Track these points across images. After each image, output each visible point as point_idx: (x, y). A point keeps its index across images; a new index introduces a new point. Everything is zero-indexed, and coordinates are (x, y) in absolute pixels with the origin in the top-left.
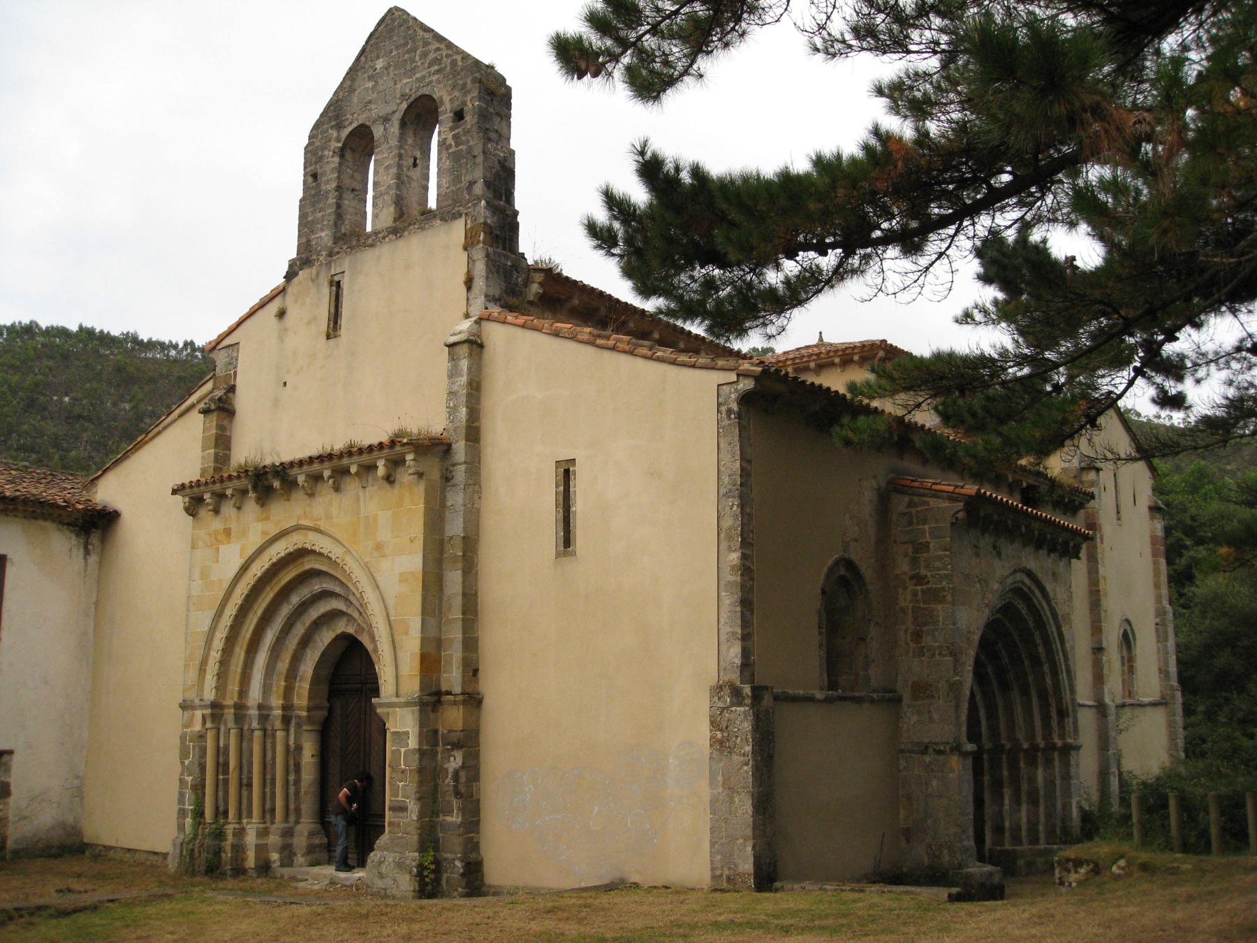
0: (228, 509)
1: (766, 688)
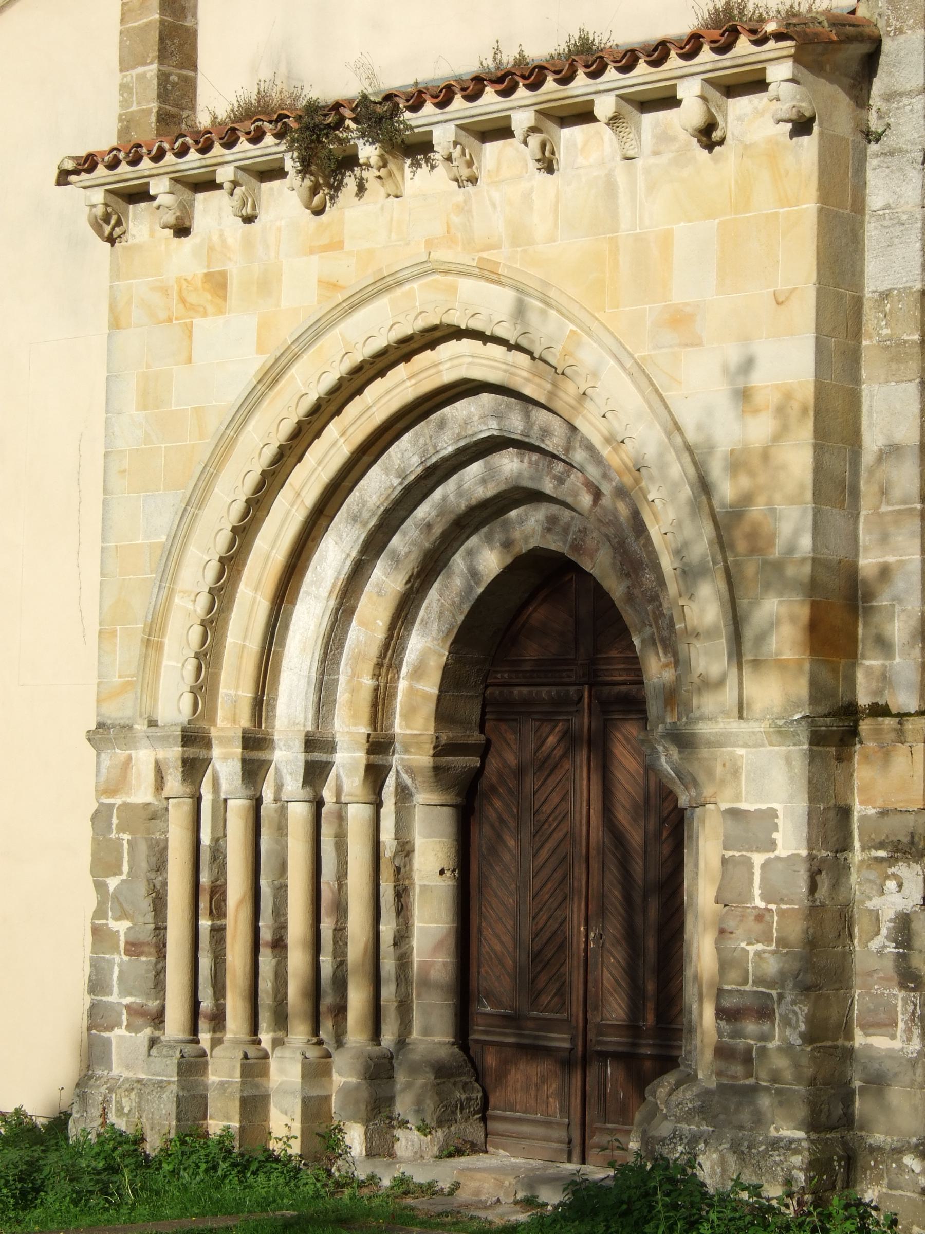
0: (213, 212)
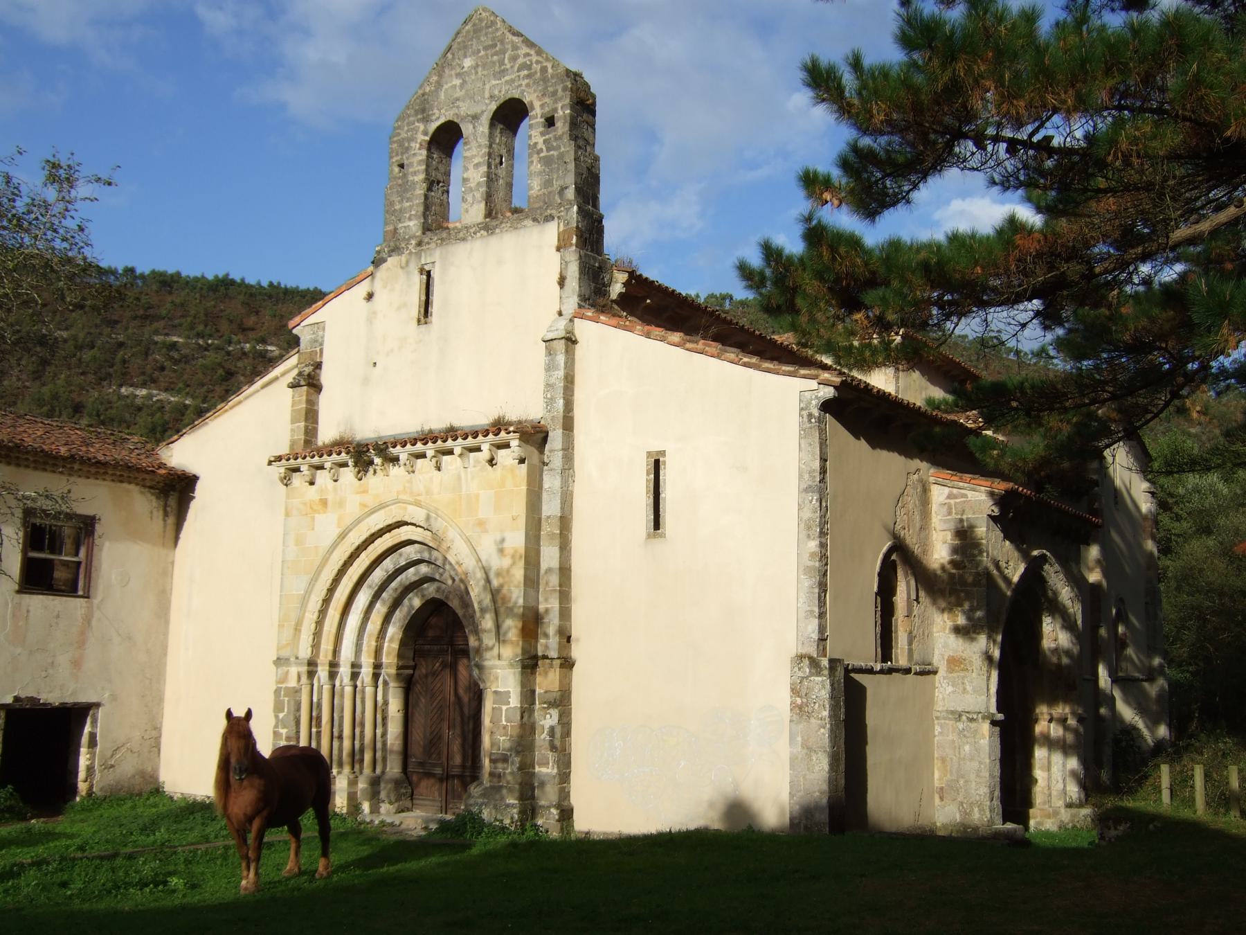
0: (323, 477)
1: (839, 660)
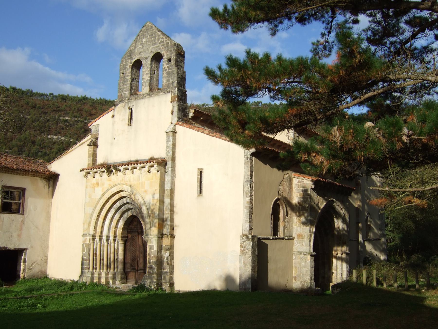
0: (97, 175)
1: (256, 236)
